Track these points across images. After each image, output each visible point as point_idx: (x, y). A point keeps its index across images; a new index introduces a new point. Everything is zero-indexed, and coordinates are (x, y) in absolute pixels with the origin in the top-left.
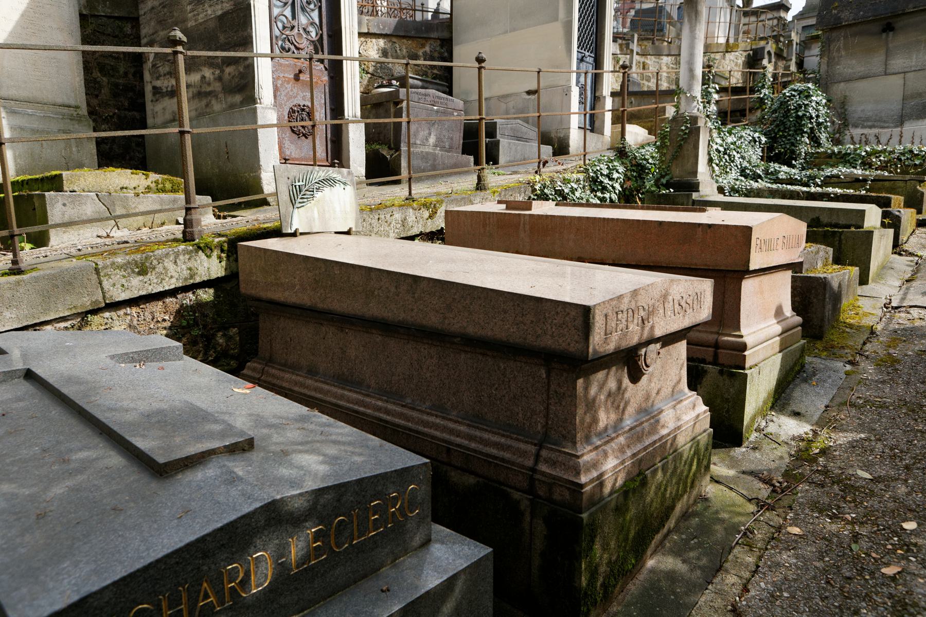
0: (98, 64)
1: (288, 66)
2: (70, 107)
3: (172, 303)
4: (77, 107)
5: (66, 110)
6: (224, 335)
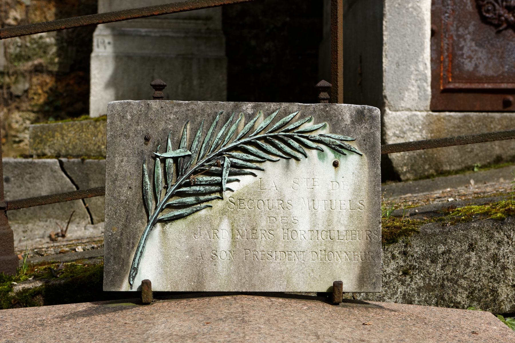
2: (197, 18)
4: (208, 18)
5: (191, 25)
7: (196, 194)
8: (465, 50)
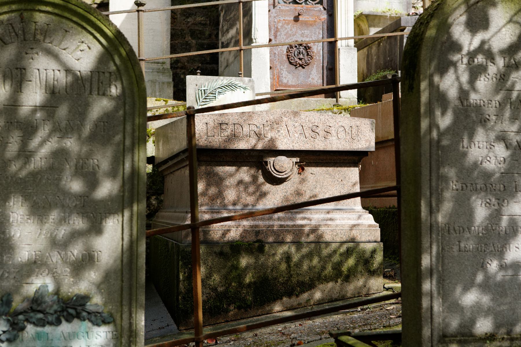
0: (191, 30)
1: (288, 11)
2: (158, 63)
3: (269, 318)
4: (163, 63)
5: (155, 66)
6: (157, 199)
7: (210, 99)
8: (283, 75)
